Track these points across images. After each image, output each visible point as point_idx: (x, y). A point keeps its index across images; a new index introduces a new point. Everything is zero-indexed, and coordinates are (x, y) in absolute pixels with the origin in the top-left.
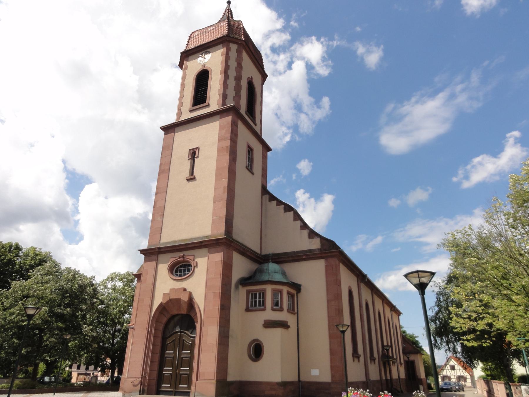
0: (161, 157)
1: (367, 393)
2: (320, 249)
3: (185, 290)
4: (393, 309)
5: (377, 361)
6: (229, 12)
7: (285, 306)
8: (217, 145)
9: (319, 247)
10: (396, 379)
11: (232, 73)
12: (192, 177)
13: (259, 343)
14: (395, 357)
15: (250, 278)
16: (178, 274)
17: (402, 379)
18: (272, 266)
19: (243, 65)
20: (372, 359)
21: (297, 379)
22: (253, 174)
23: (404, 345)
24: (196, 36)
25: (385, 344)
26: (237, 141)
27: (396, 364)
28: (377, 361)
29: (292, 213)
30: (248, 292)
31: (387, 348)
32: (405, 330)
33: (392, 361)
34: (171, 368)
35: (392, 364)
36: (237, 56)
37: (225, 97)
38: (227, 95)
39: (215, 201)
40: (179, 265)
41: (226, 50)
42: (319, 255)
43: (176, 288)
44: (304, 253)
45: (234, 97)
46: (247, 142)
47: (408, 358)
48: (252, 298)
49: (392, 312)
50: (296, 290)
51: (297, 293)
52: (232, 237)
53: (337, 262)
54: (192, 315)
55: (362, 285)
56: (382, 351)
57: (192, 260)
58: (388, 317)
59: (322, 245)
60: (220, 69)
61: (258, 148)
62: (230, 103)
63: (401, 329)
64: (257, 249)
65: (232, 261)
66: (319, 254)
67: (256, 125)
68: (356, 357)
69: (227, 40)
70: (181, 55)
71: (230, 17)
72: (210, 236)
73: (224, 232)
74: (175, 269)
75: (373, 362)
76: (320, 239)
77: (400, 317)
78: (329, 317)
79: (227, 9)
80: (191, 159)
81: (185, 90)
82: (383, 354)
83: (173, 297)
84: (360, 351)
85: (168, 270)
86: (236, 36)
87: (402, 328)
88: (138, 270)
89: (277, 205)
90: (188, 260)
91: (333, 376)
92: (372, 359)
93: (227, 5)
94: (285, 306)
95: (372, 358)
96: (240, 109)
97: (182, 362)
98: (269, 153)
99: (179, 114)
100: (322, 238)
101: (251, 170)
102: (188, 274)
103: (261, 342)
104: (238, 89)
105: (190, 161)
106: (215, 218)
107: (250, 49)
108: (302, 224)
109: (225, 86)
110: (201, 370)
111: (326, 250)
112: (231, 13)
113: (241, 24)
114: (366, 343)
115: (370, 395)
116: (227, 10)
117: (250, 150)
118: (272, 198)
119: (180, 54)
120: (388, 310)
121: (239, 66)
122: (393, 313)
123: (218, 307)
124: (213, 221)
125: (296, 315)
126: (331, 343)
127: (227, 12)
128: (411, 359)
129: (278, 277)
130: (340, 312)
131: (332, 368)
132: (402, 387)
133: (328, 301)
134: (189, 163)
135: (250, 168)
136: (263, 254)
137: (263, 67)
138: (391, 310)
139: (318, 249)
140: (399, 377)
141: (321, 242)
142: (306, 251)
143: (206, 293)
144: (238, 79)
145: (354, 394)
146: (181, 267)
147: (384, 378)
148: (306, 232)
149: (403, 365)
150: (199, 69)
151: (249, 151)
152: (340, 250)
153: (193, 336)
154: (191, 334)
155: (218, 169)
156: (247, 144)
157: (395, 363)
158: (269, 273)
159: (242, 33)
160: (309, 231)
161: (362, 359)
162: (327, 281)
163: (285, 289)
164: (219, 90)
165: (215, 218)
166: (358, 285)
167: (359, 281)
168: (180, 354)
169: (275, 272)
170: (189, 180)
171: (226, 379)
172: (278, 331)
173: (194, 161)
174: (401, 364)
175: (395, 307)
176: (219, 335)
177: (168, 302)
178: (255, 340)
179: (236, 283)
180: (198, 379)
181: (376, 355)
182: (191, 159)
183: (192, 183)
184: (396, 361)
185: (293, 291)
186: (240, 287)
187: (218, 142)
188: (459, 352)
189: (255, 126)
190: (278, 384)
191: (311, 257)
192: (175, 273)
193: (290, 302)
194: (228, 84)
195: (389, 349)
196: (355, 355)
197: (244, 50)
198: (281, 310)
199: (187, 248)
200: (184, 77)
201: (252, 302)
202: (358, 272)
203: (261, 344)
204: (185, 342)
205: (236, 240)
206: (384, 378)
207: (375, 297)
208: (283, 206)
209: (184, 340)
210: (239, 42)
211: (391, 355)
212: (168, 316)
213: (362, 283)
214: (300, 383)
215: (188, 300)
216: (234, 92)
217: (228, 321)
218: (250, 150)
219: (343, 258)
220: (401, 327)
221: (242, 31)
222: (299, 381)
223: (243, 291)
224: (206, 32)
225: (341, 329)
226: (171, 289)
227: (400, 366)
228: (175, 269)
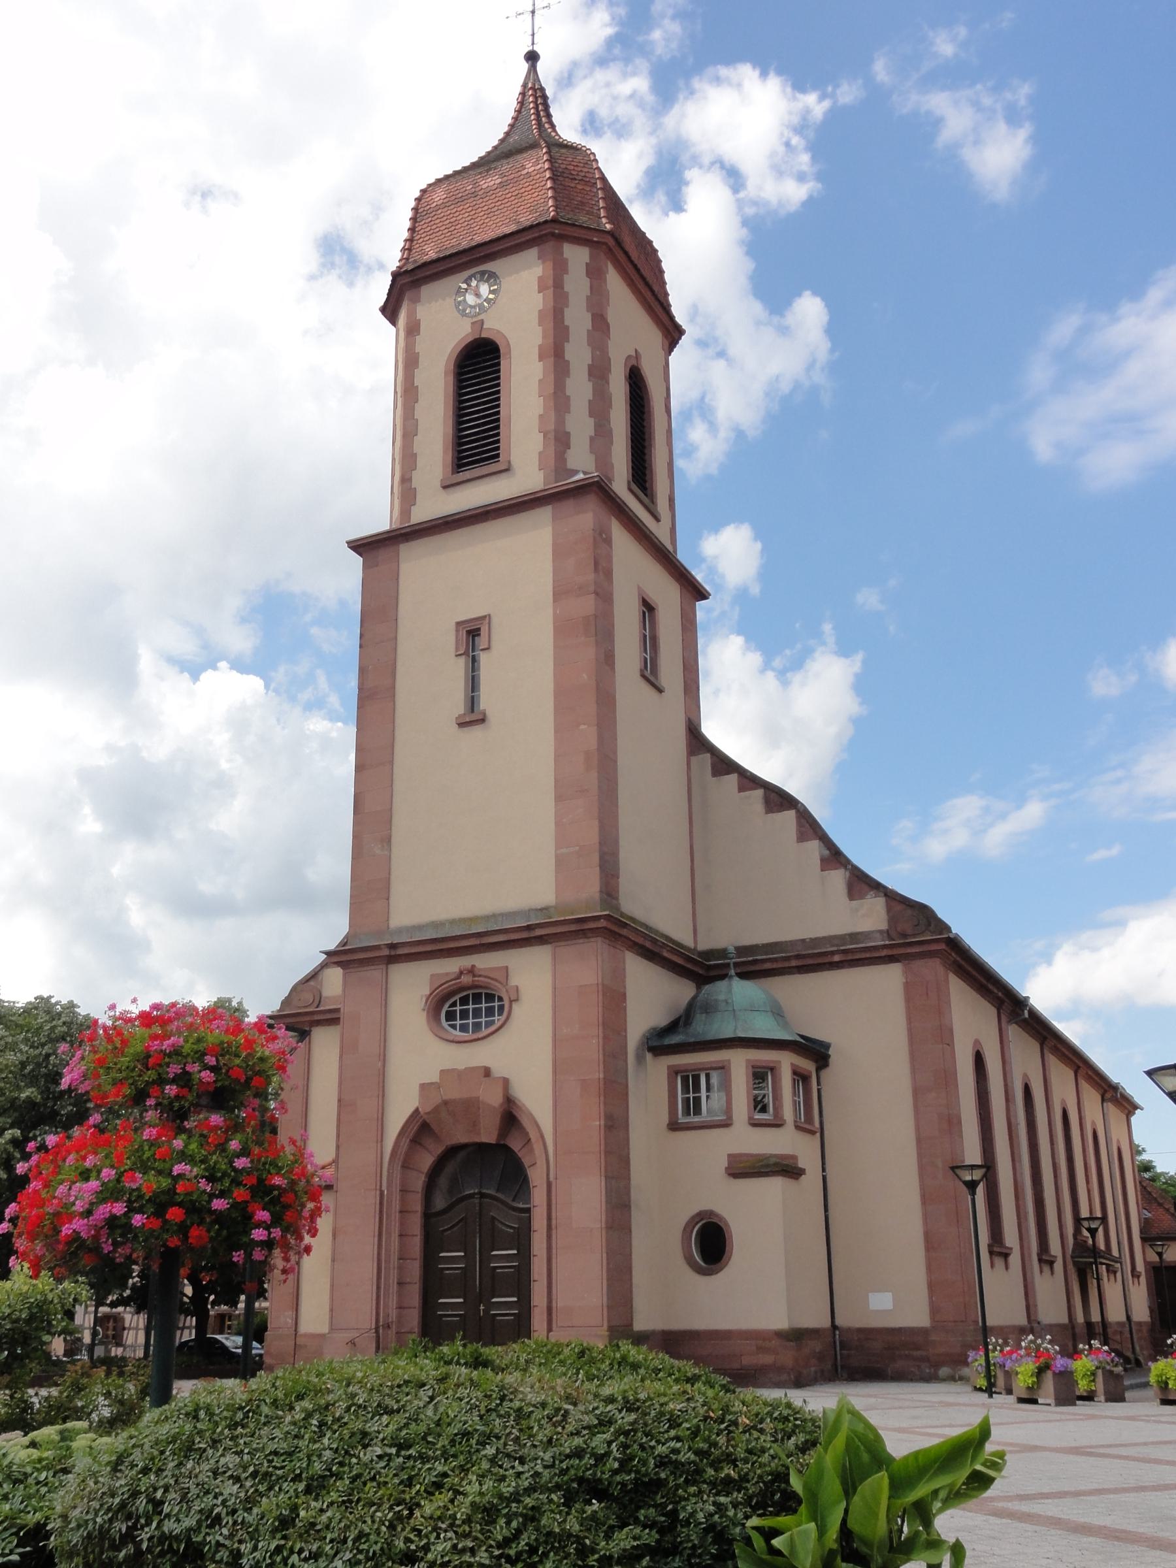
0: (361, 646)
1: (1045, 1345)
2: (888, 931)
3: (487, 1072)
4: (1108, 1096)
5: (1058, 1266)
6: (536, 98)
7: (788, 1113)
8: (550, 611)
9: (884, 926)
10: (1119, 1324)
11: (579, 354)
12: (473, 717)
13: (709, 1223)
14: (1115, 1253)
15: (672, 1027)
16: (456, 1025)
17: (1140, 1324)
18: (741, 991)
19: (610, 319)
20: (1046, 1260)
21: (826, 1323)
22: (660, 690)
23: (1146, 1212)
24: (438, 207)
25: (1085, 1213)
26: (612, 594)
27: (1119, 1275)
28: (1058, 1266)
29: (791, 815)
30: (674, 1072)
31: (1093, 1226)
32: (1151, 1161)
33: (1108, 1266)
34: (515, 1299)
35: (1105, 1274)
36: (591, 288)
37: (560, 440)
38: (568, 434)
39: (559, 798)
40: (457, 997)
41: (554, 269)
42: (884, 953)
43: (461, 1067)
44: (837, 945)
45: (592, 439)
46: (639, 587)
47: (1160, 1254)
48: (686, 1089)
49: (1105, 1104)
50: (816, 1061)
51: (818, 1070)
52: (617, 908)
53: (941, 970)
54: (515, 1144)
55: (1013, 1031)
56: (1075, 1236)
57: (500, 982)
58: (1093, 1123)
59: (893, 919)
60: (539, 340)
61: (667, 594)
62: (582, 464)
63: (1139, 1158)
64: (684, 936)
65: (624, 981)
66: (885, 947)
67: (658, 520)
68: (1000, 1254)
69: (553, 234)
70: (393, 281)
71: (543, 119)
72: (555, 907)
73: (597, 896)
74: (446, 1008)
75: (1046, 1269)
76: (887, 901)
77: (1133, 1119)
78: (919, 1141)
79: (530, 85)
80: (466, 653)
81: (420, 411)
82: (1080, 1245)
83: (453, 1093)
84: (1011, 1238)
85: (425, 1013)
86: (583, 219)
87: (1139, 1153)
88: (283, 1003)
89: (741, 789)
90: (489, 981)
91: (934, 1310)
92: (1046, 1260)
93: (525, 66)
94: (788, 1113)
95: (1044, 1257)
96: (610, 480)
97: (494, 1283)
98: (701, 605)
99: (406, 491)
100: (894, 899)
101: (652, 678)
102: (488, 1024)
103: (717, 1215)
104: (599, 409)
105: (462, 660)
106: (564, 851)
107: (626, 253)
108: (827, 852)
109: (559, 400)
110: (560, 1302)
111: (905, 936)
112: (545, 97)
113: (589, 152)
114: (1026, 1213)
115: (1055, 1350)
116: (530, 92)
117: (648, 608)
118: (724, 765)
119: (391, 278)
120: (1091, 1098)
121: (600, 324)
122: (1111, 1108)
123: (597, 1123)
124: (560, 862)
125: (818, 1135)
126: (926, 1217)
127: (531, 99)
128: (1168, 1260)
129: (764, 1027)
130: (952, 1123)
131: (932, 1287)
132: (1137, 1348)
133: (917, 1092)
134: (460, 667)
135: (650, 675)
136: (703, 946)
137: (667, 301)
138: (1103, 1100)
139: (881, 932)
140: (1128, 1318)
141: (889, 909)
142: (842, 938)
143: (555, 1082)
144: (599, 372)
145: (1004, 1355)
146: (464, 1001)
147: (1080, 1318)
148: (838, 877)
149: (1143, 1279)
150: (459, 333)
151: (644, 613)
152: (951, 936)
153: (521, 1206)
154: (514, 1200)
155: (560, 693)
156: (639, 594)
157: (1115, 1273)
158: (735, 1016)
159: (601, 204)
160: (848, 874)
161: (1015, 1259)
162: (910, 1031)
163: (786, 1062)
164: (541, 416)
165: (564, 851)
166: (1000, 1030)
167: (1003, 1018)
168: (485, 1259)
169: (753, 1009)
170: (462, 725)
171: (631, 1325)
172: (776, 1185)
173: (474, 660)
174: (1135, 1274)
175: (1114, 1088)
176: (607, 1202)
177: (436, 1110)
178: (700, 1215)
179: (638, 1049)
180: (554, 1325)
181: (1055, 1248)
182: (466, 653)
183: (476, 732)
184: (1118, 1265)
185: (808, 1065)
186: (649, 1056)
187: (554, 601)
188: (49, 1392)
189: (655, 522)
190: (779, 1334)
191: (858, 956)
192: (447, 1020)
193: (799, 1097)
194: (567, 394)
195: (1096, 1229)
196: (996, 1249)
197: (609, 264)
198: (777, 1124)
199: (483, 945)
200: (409, 362)
201: (686, 1101)
202: (1000, 994)
203: (715, 1220)
204: (500, 1226)
205: (630, 914)
206: (1080, 1318)
207: (1052, 1060)
208: (759, 793)
209: (493, 1218)
210: (595, 239)
211: (1102, 1247)
212: (440, 1150)
213: (1014, 1025)
214: (837, 1332)
215: (502, 1105)
216: (591, 421)
217: (625, 1161)
218: (648, 608)
219: (958, 959)
220: (1136, 1151)
221: (600, 194)
222: (834, 1327)
223: (659, 1069)
224: (474, 194)
225: (968, 1178)
226: (442, 1072)
227: (1131, 1282)
228: (446, 1008)
